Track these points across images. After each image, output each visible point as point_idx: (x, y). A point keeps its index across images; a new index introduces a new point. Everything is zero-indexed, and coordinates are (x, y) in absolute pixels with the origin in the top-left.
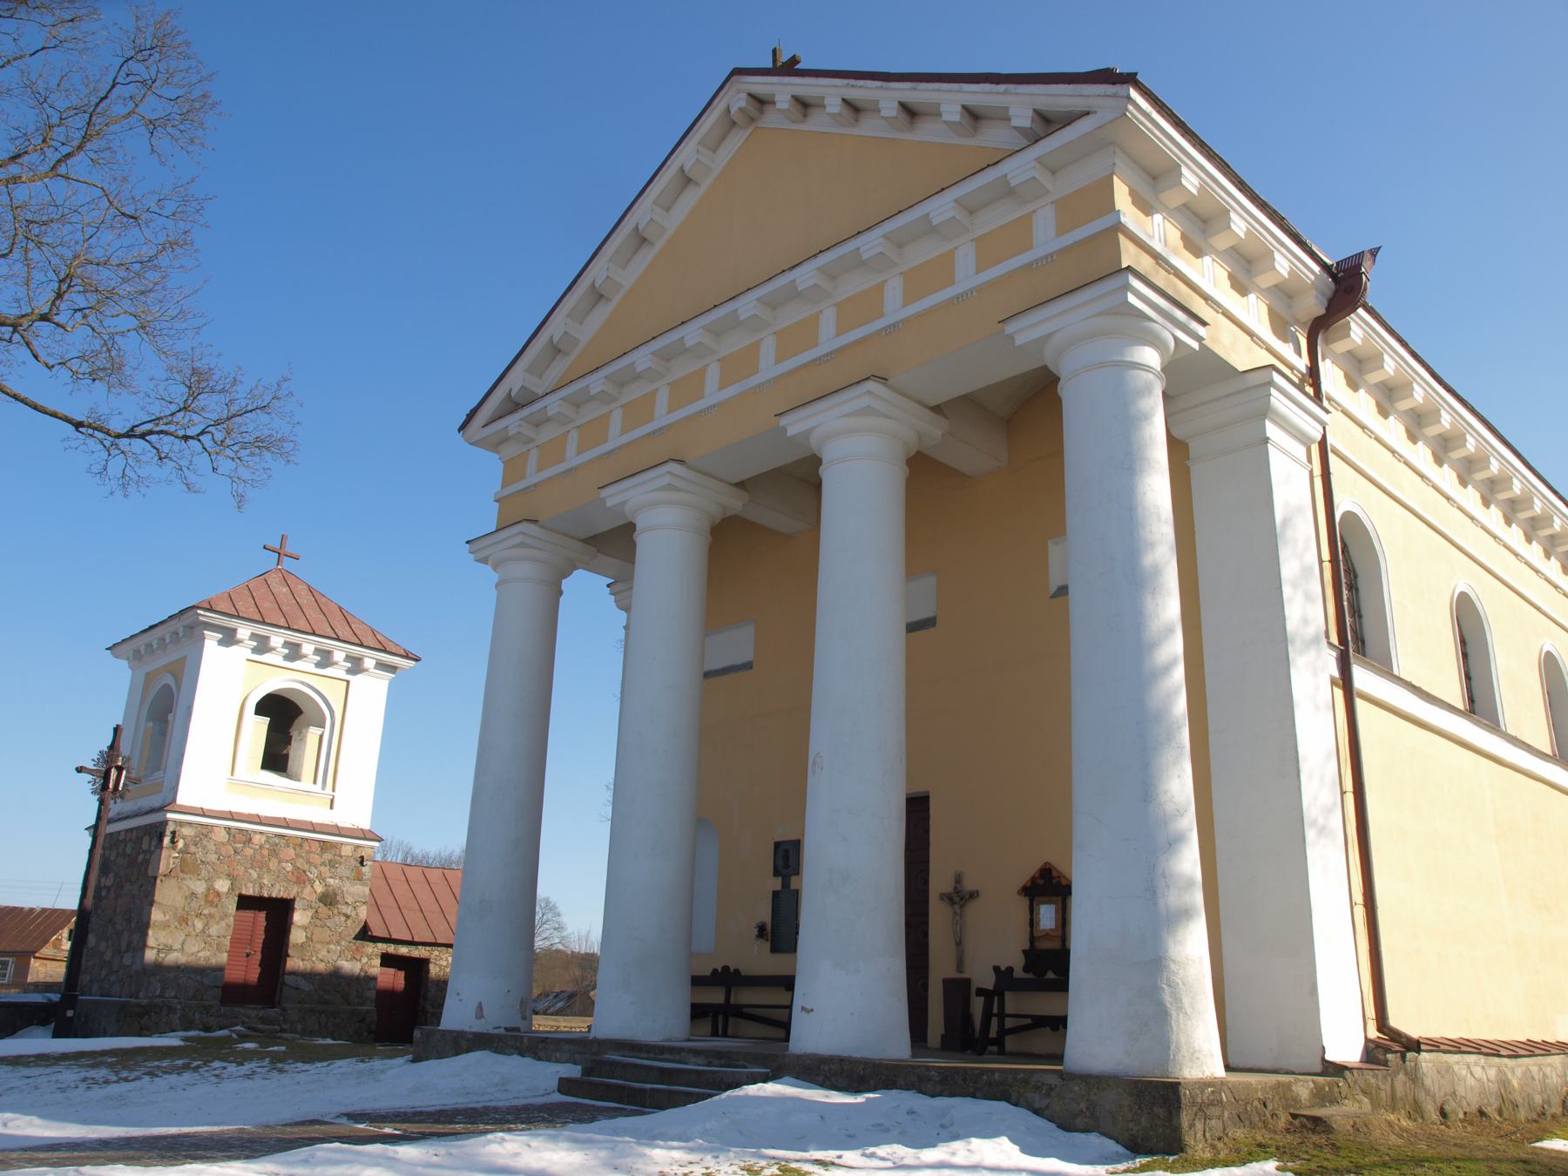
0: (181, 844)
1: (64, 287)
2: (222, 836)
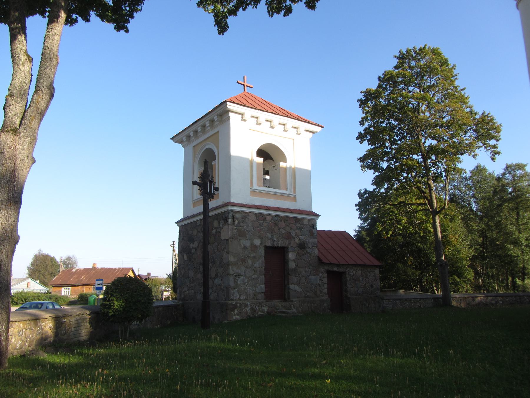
0: (236, 222)
2: (254, 218)
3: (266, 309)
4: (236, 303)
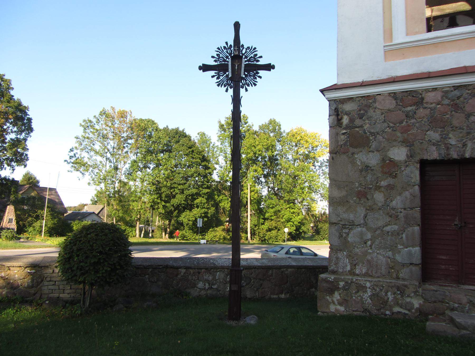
0: (345, 120)
1: (271, 206)
2: (390, 104)
3: (417, 303)
4: (337, 281)
